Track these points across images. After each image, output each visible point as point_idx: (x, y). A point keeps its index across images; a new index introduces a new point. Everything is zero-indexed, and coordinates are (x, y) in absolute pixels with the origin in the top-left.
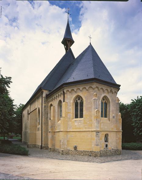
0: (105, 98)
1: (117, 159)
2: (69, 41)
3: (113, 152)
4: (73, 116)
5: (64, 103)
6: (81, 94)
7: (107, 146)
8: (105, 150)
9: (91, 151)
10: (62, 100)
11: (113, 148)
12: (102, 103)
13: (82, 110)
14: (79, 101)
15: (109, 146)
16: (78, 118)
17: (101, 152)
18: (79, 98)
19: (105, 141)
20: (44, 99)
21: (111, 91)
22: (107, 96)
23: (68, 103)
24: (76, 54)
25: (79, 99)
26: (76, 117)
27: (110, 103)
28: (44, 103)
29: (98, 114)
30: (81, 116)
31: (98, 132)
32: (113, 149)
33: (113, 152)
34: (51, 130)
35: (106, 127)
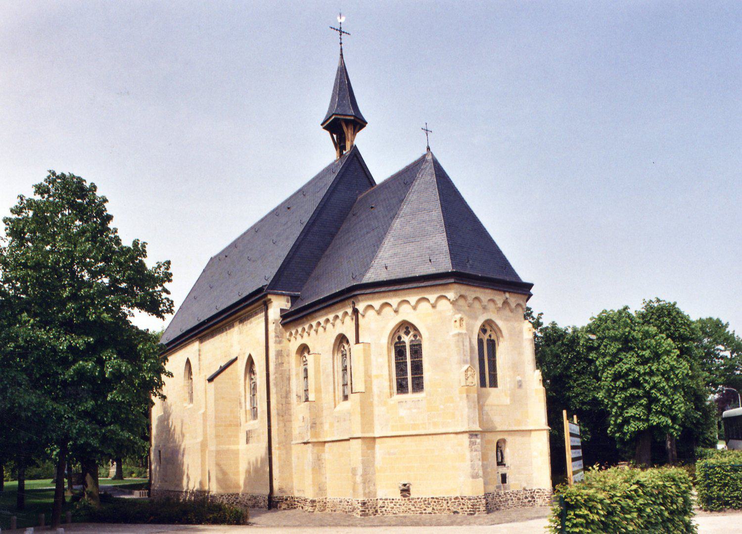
0: (487, 326)
1: (536, 516)
2: (348, 122)
4: (391, 387)
5: (360, 347)
9: (456, 498)
10: (351, 337)
12: (480, 342)
13: (418, 368)
14: (407, 339)
17: (490, 500)
18: (407, 328)
20: (276, 329)
21: (506, 303)
22: (494, 319)
23: (373, 346)
24: (380, 171)
25: (407, 333)
26: (402, 388)
28: (276, 342)
30: (418, 384)
32: (525, 489)
33: (526, 498)
34: (313, 436)
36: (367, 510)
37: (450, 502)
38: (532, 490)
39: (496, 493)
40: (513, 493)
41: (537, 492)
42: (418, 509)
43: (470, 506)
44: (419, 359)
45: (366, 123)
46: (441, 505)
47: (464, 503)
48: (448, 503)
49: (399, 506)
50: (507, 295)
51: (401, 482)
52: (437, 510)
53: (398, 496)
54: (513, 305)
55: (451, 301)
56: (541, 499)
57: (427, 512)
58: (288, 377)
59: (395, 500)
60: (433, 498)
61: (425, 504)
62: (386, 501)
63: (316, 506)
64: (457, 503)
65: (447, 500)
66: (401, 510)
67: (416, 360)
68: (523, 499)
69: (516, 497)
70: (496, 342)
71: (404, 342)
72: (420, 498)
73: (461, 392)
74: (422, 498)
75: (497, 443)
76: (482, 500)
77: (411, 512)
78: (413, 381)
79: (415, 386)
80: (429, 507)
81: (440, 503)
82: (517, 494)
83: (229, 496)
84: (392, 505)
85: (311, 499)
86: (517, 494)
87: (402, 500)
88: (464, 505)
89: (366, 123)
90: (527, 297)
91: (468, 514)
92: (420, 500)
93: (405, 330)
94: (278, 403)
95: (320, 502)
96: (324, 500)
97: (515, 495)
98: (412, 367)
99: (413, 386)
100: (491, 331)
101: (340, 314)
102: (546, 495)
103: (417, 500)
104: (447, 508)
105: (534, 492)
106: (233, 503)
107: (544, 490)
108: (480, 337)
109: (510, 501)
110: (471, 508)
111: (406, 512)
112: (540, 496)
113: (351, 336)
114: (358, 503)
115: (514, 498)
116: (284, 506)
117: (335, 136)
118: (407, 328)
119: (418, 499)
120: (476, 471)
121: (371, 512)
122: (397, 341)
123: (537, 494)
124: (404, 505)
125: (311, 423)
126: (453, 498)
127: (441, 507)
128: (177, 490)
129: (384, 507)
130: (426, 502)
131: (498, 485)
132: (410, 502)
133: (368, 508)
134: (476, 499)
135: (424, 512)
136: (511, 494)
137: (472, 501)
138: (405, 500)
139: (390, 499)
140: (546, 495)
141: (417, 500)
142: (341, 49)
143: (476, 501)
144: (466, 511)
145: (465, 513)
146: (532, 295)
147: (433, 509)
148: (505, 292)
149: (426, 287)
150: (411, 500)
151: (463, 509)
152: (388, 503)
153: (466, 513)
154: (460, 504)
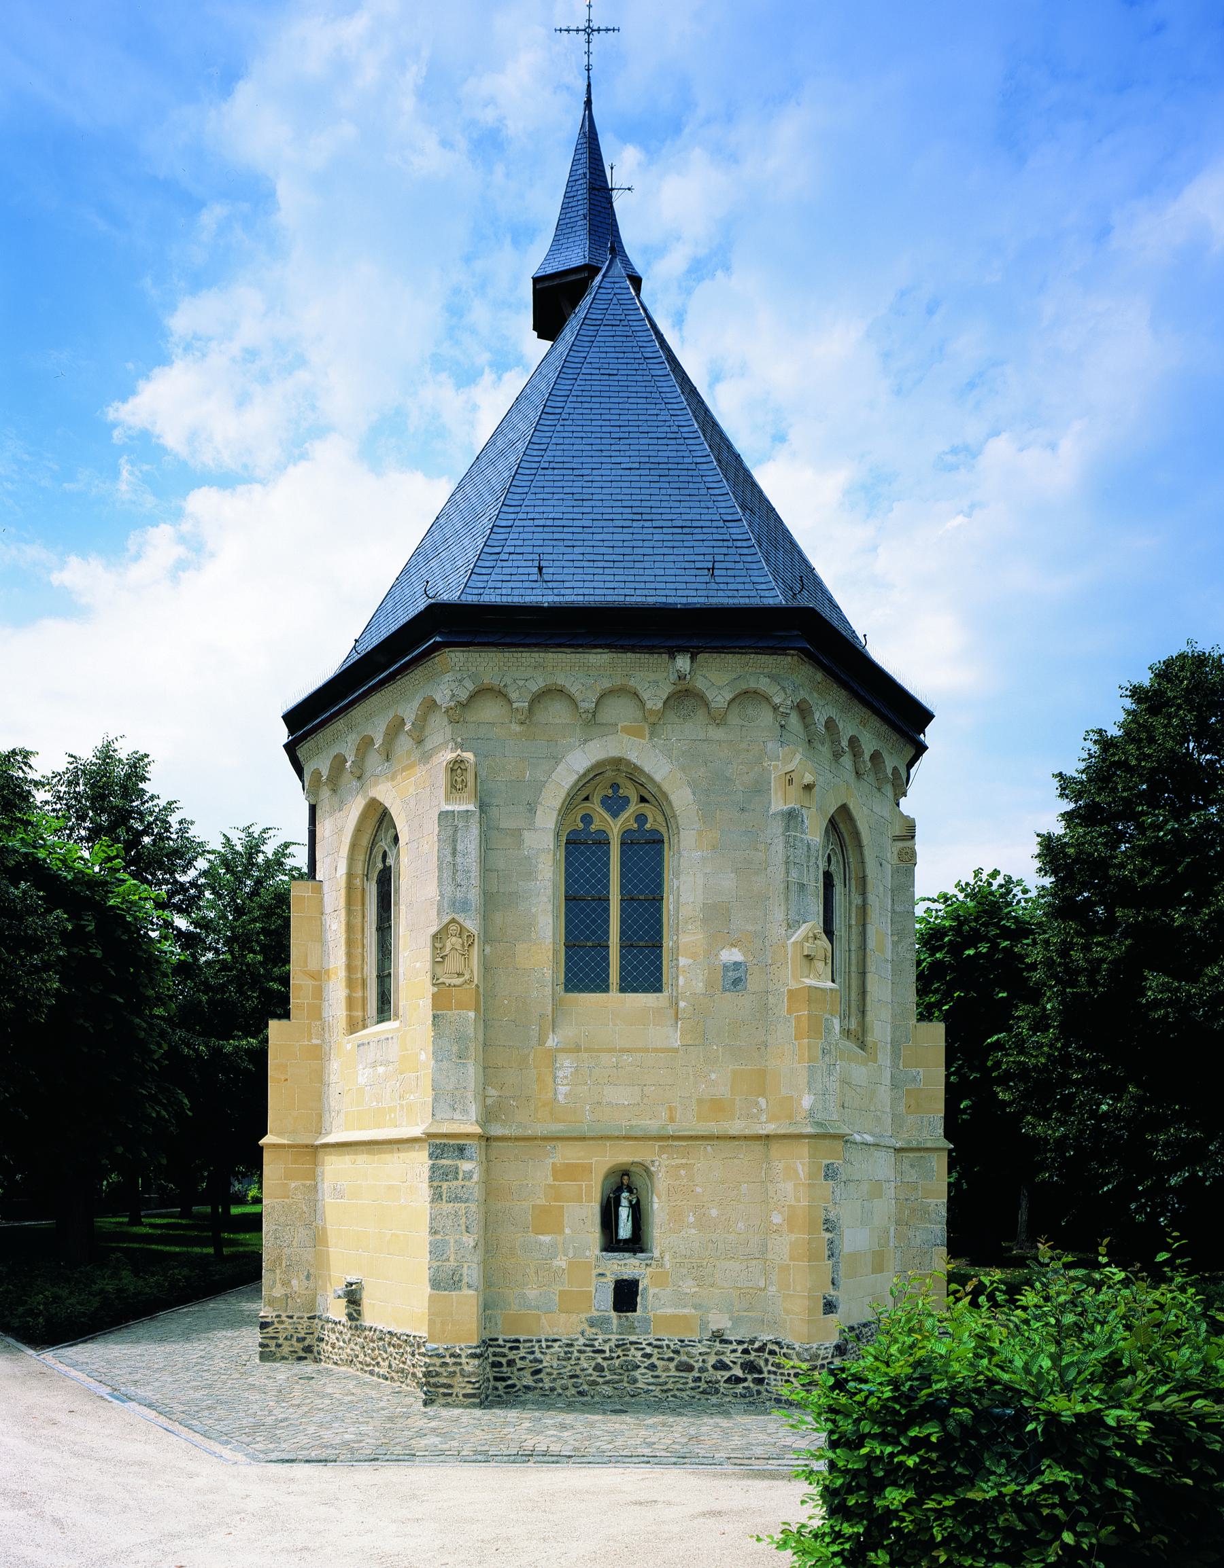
3: (721, 1366)
11: (719, 1321)
16: (606, 989)
19: (612, 1244)
22: (633, 757)
27: (860, 846)
29: (455, 963)
31: (461, 1149)
35: (620, 1095)
39: (582, 1341)
50: (683, 662)
54: (719, 698)
68: (702, 1370)
69: (671, 1359)
82: (677, 1352)
105: (761, 1349)
120: (453, 1263)
123: (771, 1359)
131: (596, 1314)
134: (439, 1356)
136: (649, 1350)
142: (589, 77)
143: (438, 1361)
148: (672, 652)
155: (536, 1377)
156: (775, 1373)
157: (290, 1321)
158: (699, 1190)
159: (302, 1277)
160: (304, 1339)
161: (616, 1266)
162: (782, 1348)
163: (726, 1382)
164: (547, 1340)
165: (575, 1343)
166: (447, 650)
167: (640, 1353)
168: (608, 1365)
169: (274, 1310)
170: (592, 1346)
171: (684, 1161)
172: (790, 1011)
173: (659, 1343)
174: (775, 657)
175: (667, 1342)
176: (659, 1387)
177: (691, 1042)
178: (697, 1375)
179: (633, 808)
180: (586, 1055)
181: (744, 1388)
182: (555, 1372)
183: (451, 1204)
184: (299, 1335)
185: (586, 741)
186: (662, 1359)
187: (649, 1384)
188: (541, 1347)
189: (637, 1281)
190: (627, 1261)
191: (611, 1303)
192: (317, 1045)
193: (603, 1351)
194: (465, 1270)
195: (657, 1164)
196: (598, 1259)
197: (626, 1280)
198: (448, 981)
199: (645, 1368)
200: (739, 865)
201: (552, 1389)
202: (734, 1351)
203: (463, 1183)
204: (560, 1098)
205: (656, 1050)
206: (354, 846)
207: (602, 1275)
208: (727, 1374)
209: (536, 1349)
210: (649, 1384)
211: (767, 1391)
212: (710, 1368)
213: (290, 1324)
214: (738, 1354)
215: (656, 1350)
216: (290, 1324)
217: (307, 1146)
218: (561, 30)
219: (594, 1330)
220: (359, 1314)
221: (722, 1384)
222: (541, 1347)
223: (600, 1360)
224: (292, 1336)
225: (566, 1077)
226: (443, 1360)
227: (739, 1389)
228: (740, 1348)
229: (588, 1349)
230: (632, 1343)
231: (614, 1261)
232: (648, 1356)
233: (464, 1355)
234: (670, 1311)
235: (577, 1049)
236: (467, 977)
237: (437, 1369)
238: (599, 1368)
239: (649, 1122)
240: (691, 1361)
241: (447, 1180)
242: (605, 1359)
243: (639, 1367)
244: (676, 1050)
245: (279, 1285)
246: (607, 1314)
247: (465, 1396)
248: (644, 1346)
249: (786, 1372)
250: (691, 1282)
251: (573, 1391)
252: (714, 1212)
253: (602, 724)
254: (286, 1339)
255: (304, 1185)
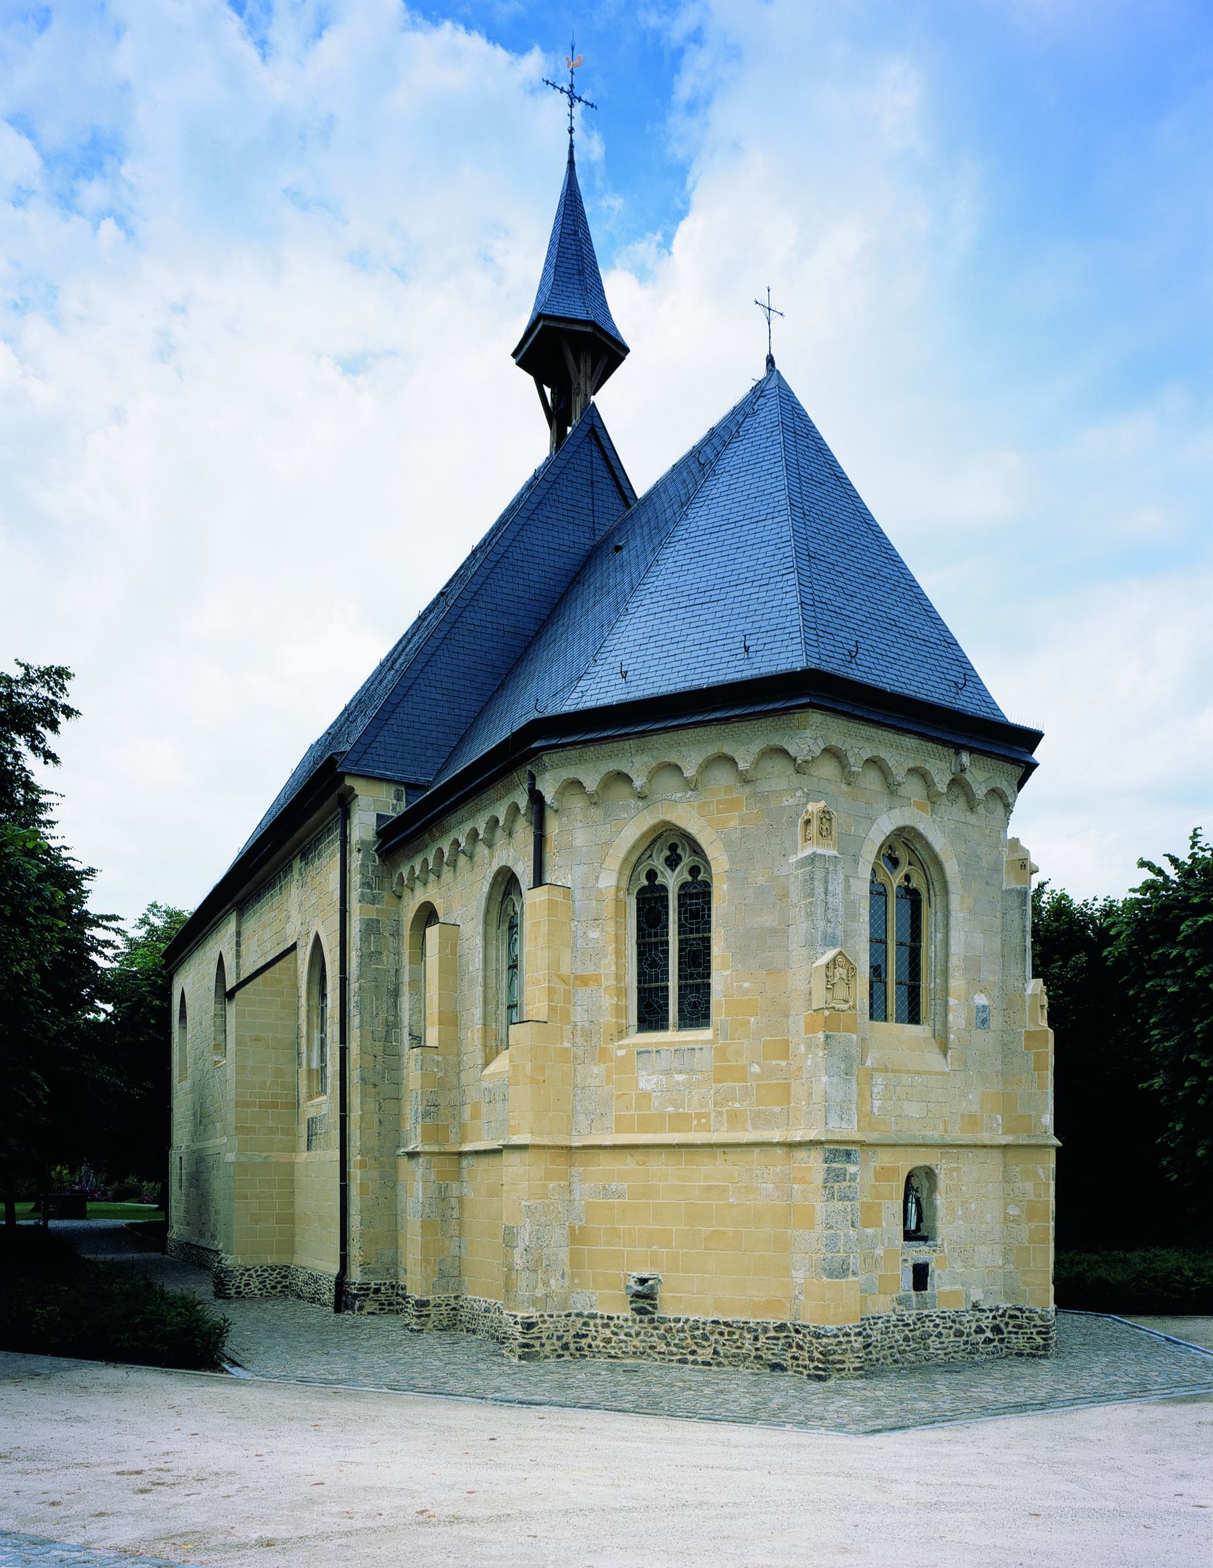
3: (979, 1330)
4: (620, 1011)
6: (688, 818)
7: (921, 1275)
8: (910, 1315)
9: (781, 1327)
10: (524, 873)
11: (977, 1295)
12: (878, 892)
14: (672, 881)
15: (938, 1281)
18: (673, 848)
19: (909, 1236)
21: (958, 783)
22: (921, 828)
30: (694, 1005)
31: (848, 1154)
32: (975, 1306)
33: (979, 1330)
35: (914, 1110)
36: (537, 1343)
37: (762, 1338)
38: (997, 1309)
39: (894, 1317)
40: (944, 1318)
41: (1011, 1317)
42: (674, 1349)
43: (817, 1355)
44: (700, 935)
45: (627, 351)
46: (739, 1344)
47: (801, 1343)
48: (756, 1339)
49: (625, 1338)
51: (634, 1274)
52: (726, 1357)
53: (624, 1312)
55: (799, 761)
56: (1020, 1336)
57: (700, 1359)
58: (391, 987)
59: (616, 1321)
60: (715, 1322)
61: (693, 1337)
62: (592, 1323)
63: (428, 1316)
64: (783, 1341)
65: (756, 1330)
66: (630, 1349)
67: (692, 936)
69: (951, 1328)
70: (924, 896)
71: (664, 888)
72: (683, 1320)
73: (810, 1029)
74: (687, 1321)
75: (909, 1177)
76: (853, 1338)
77: (656, 1356)
78: (681, 997)
79: (687, 1009)
80: (704, 1347)
81: (735, 1337)
83: (265, 1270)
84: (607, 1333)
85: (417, 1297)
86: (954, 1321)
87: (634, 1321)
88: (800, 1347)
89: (627, 351)
90: (1019, 771)
91: (808, 1375)
92: (681, 1324)
93: (668, 853)
94: (363, 1052)
95: (440, 1305)
96: (452, 1302)
97: (950, 1324)
98: (680, 957)
99: (680, 1011)
100: (910, 864)
101: (501, 812)
102: (1035, 1326)
103: (673, 1325)
104: (753, 1354)
106: (274, 1288)
107: (1030, 1312)
108: (880, 878)
109: (933, 1338)
110: (819, 1360)
111: (642, 1353)
112: (1020, 1327)
113: (524, 872)
114: (516, 1323)
115: (944, 1331)
116: (370, 1306)
117: (548, 391)
118: (673, 848)
119: (677, 1320)
121: (548, 1348)
122: (646, 883)
123: (1012, 1322)
124: (638, 1334)
125: (425, 1103)
126: (771, 1326)
127: (738, 1348)
128: (203, 1243)
129: (585, 1336)
130: (697, 1333)
131: (902, 1293)
132: (656, 1328)
133: (540, 1338)
134: (836, 1336)
135: (691, 1358)
136: (938, 1321)
137: (825, 1340)
138: (641, 1321)
139: (602, 1318)
140: (1035, 1326)
141: (673, 1325)
142: (572, 140)
143: (834, 1341)
144: (805, 1367)
145: (801, 1373)
146: (1037, 765)
147: (716, 1352)
148: (958, 749)
149: (727, 720)
150: (656, 1324)
151: (797, 1359)
152: (596, 1326)
153: (806, 1372)
154: (790, 1346)
155: (867, 1350)
156: (1016, 1333)
157: (552, 1320)
158: (964, 1188)
159: (559, 1277)
160: (562, 1337)
161: (914, 1253)
162: (1024, 1312)
163: (983, 1343)
164: (873, 1318)
165: (891, 1319)
166: (810, 710)
167: (931, 1324)
168: (913, 1336)
169: (537, 1310)
170: (903, 1320)
171: (955, 1165)
172: (1027, 1047)
173: (943, 1315)
174: (1013, 766)
175: (948, 1314)
176: (944, 1351)
177: (957, 1068)
178: (966, 1339)
179: (904, 869)
180: (892, 1075)
181: (994, 1346)
182: (879, 1345)
183: (841, 1203)
184: (559, 1334)
185: (891, 808)
186: (946, 1328)
187: (937, 1349)
188: (870, 1324)
189: (928, 1265)
190: (921, 1248)
191: (911, 1285)
192: (567, 1048)
193: (908, 1325)
194: (851, 1260)
195: (939, 1167)
196: (903, 1247)
197: (921, 1264)
198: (837, 1006)
199: (936, 1336)
200: (986, 928)
201: (878, 1360)
202: (988, 1318)
203: (849, 1184)
204: (875, 1110)
205: (936, 1073)
206: (626, 860)
207: (905, 1260)
208: (983, 1336)
209: (867, 1326)
210: (937, 1349)
211: (1007, 1348)
212: (973, 1333)
213: (551, 1323)
214: (990, 1320)
215: (942, 1321)
216: (551, 1323)
217: (562, 1147)
218: (547, 83)
219: (901, 1307)
220: (654, 1307)
221: (980, 1344)
222: (870, 1324)
223: (907, 1332)
224: (553, 1335)
225: (879, 1093)
226: (838, 1340)
227: (990, 1348)
228: (991, 1315)
229: (901, 1323)
230: (926, 1316)
231: (914, 1248)
232: (936, 1326)
233: (852, 1334)
234: (947, 1288)
235: (886, 1070)
236: (851, 1003)
237: (834, 1347)
238: (906, 1339)
239: (931, 1132)
240: (962, 1328)
241: (838, 1181)
242: (910, 1331)
243: (932, 1335)
244: (948, 1074)
245: (540, 1285)
246: (909, 1293)
247: (854, 1369)
248: (934, 1318)
249: (1028, 1331)
250: (960, 1264)
251: (890, 1360)
252: (973, 1206)
253: (903, 797)
254: (548, 1338)
255: (559, 1185)
